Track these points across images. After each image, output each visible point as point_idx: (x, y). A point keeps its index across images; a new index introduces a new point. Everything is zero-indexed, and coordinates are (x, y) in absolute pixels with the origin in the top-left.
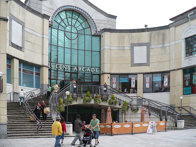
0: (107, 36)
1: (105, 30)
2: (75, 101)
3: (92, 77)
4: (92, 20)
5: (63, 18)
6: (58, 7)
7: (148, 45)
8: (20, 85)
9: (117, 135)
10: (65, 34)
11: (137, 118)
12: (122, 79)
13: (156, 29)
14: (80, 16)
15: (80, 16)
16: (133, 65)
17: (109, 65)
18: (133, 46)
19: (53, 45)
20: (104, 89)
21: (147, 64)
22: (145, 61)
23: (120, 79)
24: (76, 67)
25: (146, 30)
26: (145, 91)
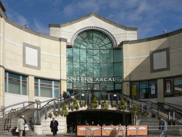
2: (84, 107)
7: (167, 50)
8: (6, 91)
10: (87, 52)
11: (150, 122)
12: (142, 85)
16: (153, 71)
19: (174, 93)
20: (114, 96)
21: (168, 69)
22: (165, 66)
25: (165, 36)
26: (166, 96)
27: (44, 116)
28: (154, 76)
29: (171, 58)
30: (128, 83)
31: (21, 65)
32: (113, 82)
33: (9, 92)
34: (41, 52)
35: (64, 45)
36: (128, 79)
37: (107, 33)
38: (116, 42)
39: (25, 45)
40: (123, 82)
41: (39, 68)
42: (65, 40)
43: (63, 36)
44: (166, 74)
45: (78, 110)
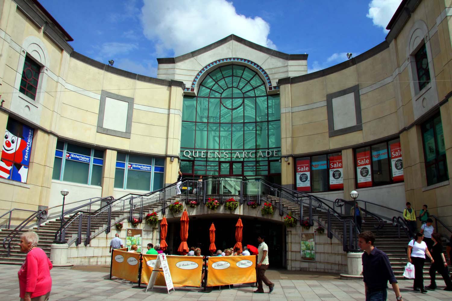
0: (286, 90)
1: (282, 82)
3: (269, 165)
4: (263, 70)
5: (252, 82)
6: (204, 66)
7: (355, 90)
8: (56, 176)
9: (85, 257)
13: (213, 47)
14: (246, 69)
15: (246, 69)
16: (334, 133)
17: (289, 140)
18: (330, 98)
21: (358, 128)
22: (353, 123)
23: (314, 164)
24: (237, 152)
25: (351, 64)
27: (105, 227)
28: (334, 144)
29: (363, 106)
30: (290, 160)
31: (95, 129)
32: (266, 159)
33: (65, 179)
34: (135, 106)
35: (178, 92)
36: (290, 153)
37: (229, 61)
38: (270, 82)
39: (106, 94)
40: (281, 157)
41: (127, 135)
42: (180, 84)
43: (177, 78)
44: (357, 138)
45: (270, 218)
